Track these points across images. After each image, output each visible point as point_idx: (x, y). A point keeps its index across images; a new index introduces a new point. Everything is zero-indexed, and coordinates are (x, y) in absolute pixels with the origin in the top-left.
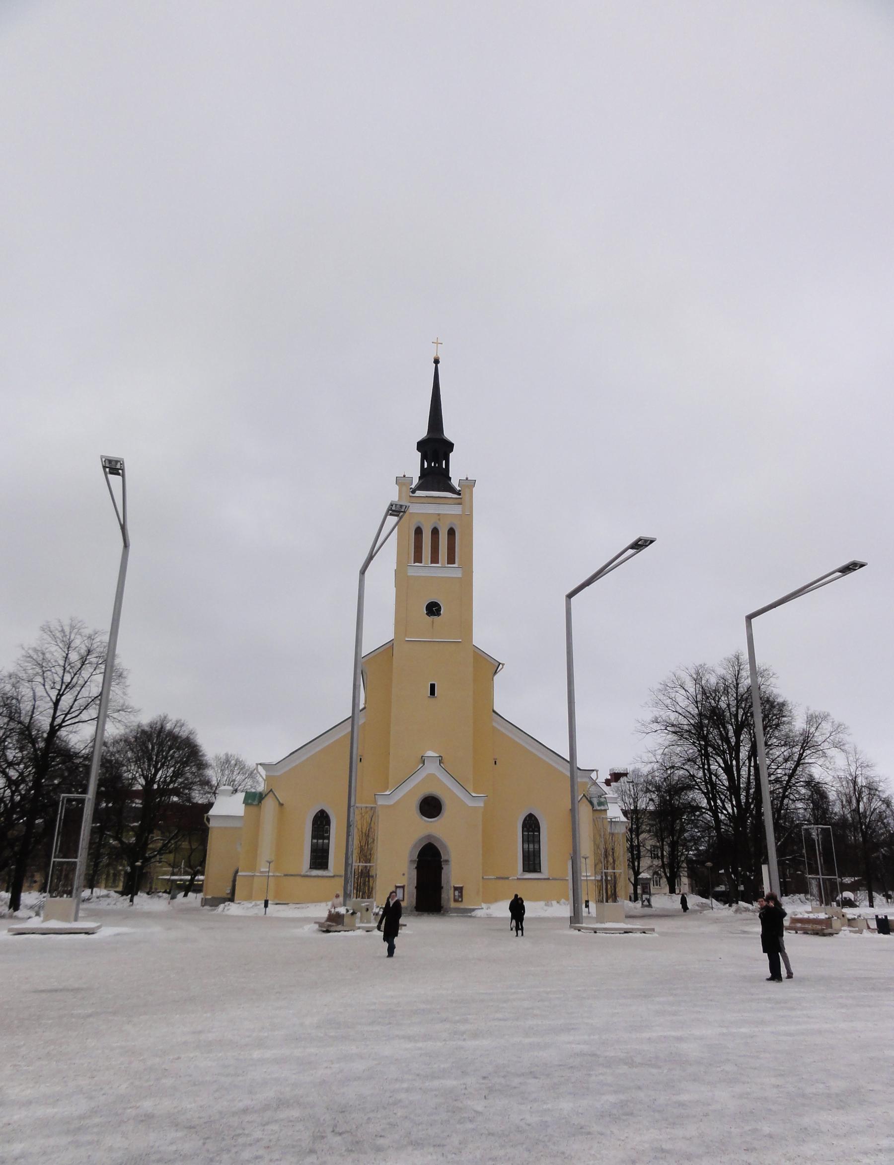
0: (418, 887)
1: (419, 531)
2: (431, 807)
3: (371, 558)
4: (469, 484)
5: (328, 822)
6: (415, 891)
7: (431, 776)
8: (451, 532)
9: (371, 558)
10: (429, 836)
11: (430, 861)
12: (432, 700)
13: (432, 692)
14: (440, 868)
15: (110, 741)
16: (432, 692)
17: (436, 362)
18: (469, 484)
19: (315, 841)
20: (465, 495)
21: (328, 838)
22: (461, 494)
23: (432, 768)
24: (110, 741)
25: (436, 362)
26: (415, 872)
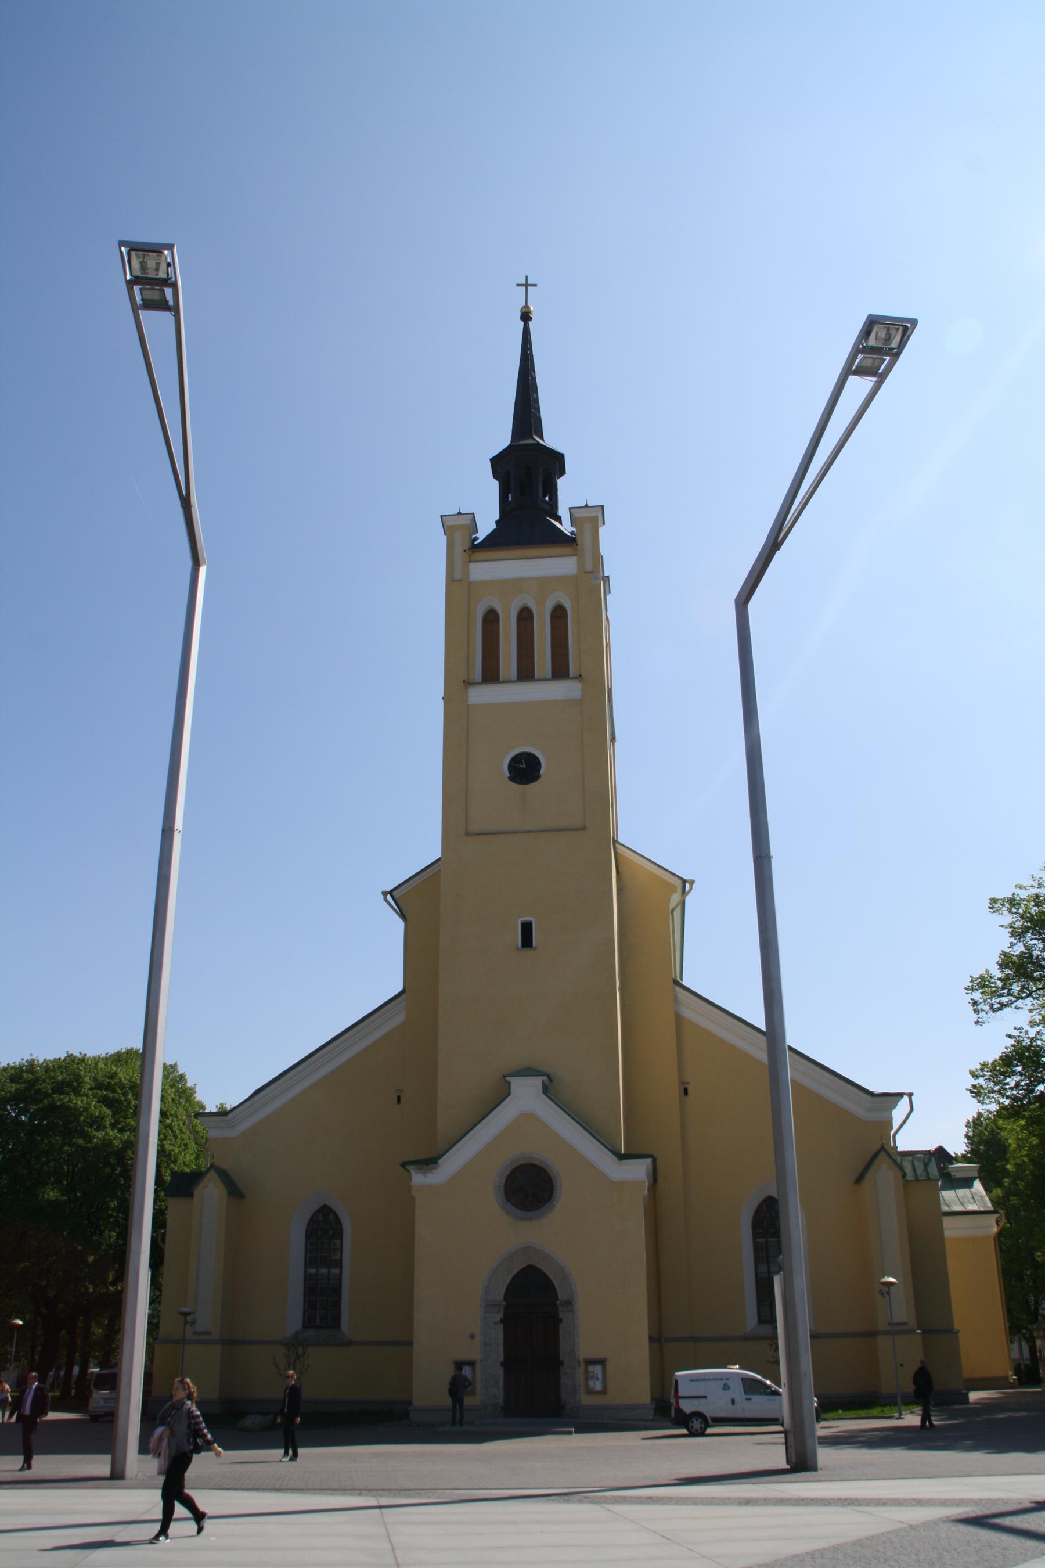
0: (509, 1364)
1: (491, 619)
3: (186, 502)
4: (591, 518)
5: (339, 1233)
6: (500, 1372)
7: (527, 1118)
8: (559, 614)
9: (186, 502)
11: (532, 1306)
12: (528, 952)
13: (527, 940)
14: (556, 1321)
15: (1019, 1350)
16: (527, 940)
17: (526, 317)
18: (591, 518)
19: (313, 1271)
20: (585, 541)
21: (339, 1264)
22: (580, 542)
23: (526, 1096)
24: (1019, 1350)
25: (526, 317)
26: (499, 1332)
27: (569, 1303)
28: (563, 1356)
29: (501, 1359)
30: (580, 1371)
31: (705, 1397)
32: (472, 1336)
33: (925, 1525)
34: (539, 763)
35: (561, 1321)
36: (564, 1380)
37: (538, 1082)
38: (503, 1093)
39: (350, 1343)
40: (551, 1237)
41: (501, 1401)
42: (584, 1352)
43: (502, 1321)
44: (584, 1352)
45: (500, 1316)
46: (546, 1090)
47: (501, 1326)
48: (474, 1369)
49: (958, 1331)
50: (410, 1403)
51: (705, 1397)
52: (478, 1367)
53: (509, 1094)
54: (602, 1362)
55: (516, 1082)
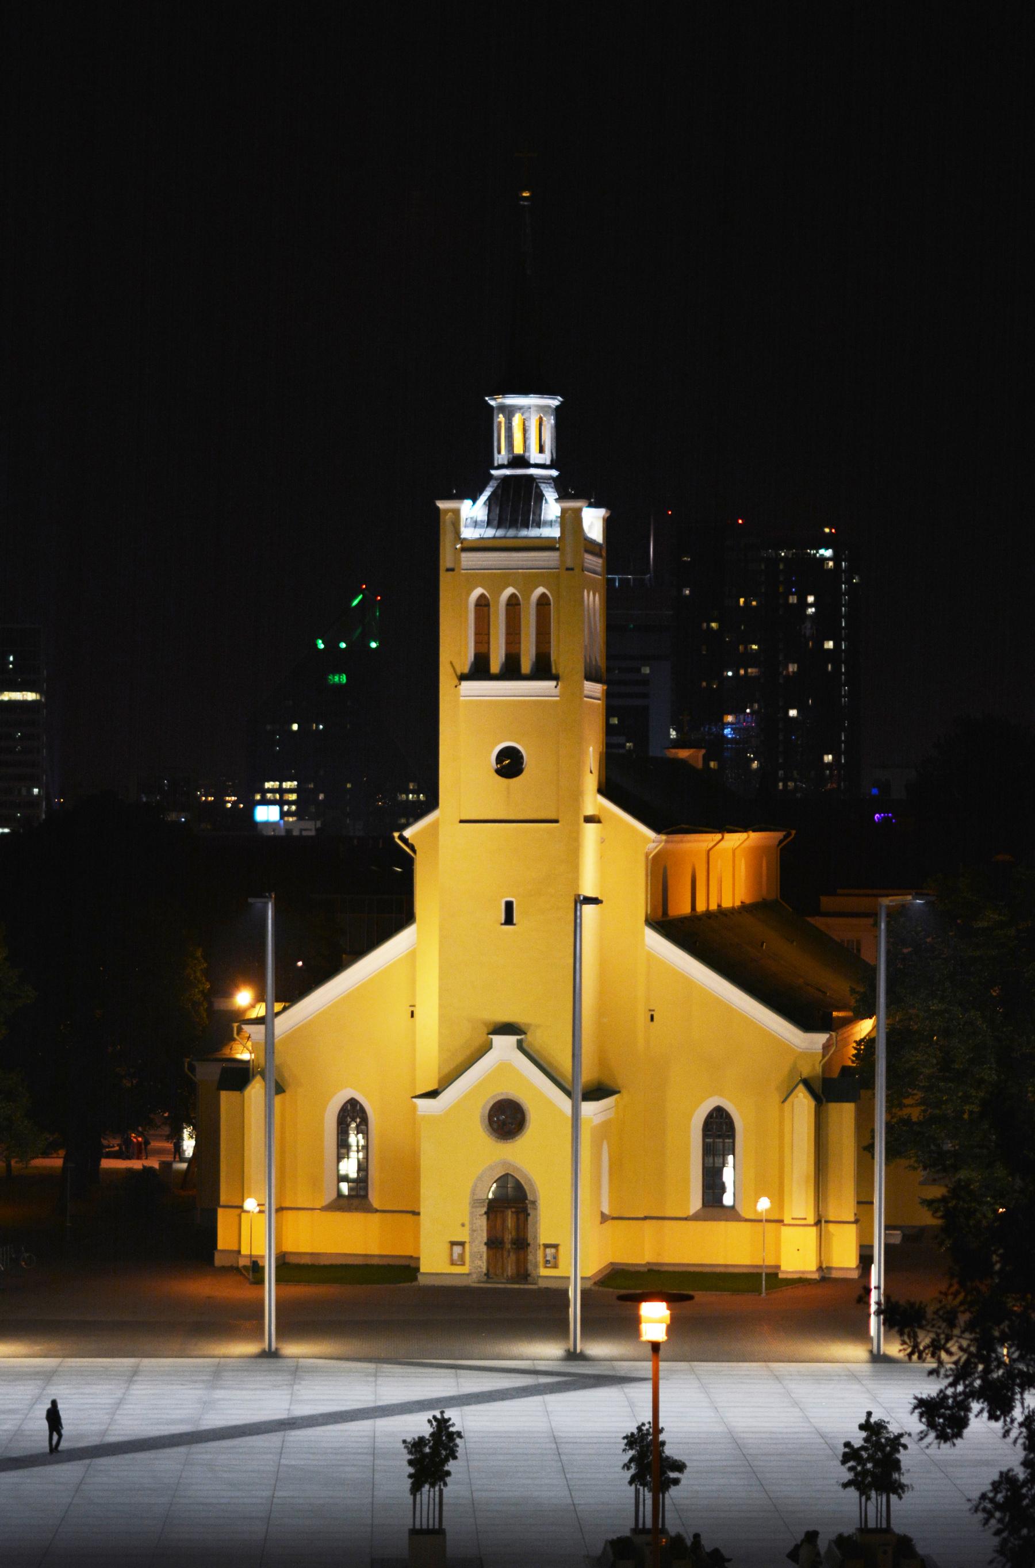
2: (507, 1119)
6: (484, 1249)
7: (504, 1068)
10: (505, 1163)
13: (509, 920)
16: (509, 920)
27: (534, 1203)
28: (530, 1240)
29: (485, 1240)
30: (540, 1253)
31: (462, 821)
32: (463, 1225)
33: (609, 1147)
34: (522, 757)
35: (529, 1215)
36: (530, 1257)
37: (513, 1039)
38: (488, 1047)
39: (377, 1211)
40: (524, 1155)
41: (484, 1270)
42: (543, 1239)
43: (486, 1213)
44: (543, 1239)
45: (485, 1209)
46: (520, 1046)
47: (485, 1217)
48: (464, 1248)
49: (1001, 1473)
50: (418, 1269)
51: (462, 821)
52: (467, 1246)
53: (491, 1048)
54: (556, 1246)
55: (497, 1039)
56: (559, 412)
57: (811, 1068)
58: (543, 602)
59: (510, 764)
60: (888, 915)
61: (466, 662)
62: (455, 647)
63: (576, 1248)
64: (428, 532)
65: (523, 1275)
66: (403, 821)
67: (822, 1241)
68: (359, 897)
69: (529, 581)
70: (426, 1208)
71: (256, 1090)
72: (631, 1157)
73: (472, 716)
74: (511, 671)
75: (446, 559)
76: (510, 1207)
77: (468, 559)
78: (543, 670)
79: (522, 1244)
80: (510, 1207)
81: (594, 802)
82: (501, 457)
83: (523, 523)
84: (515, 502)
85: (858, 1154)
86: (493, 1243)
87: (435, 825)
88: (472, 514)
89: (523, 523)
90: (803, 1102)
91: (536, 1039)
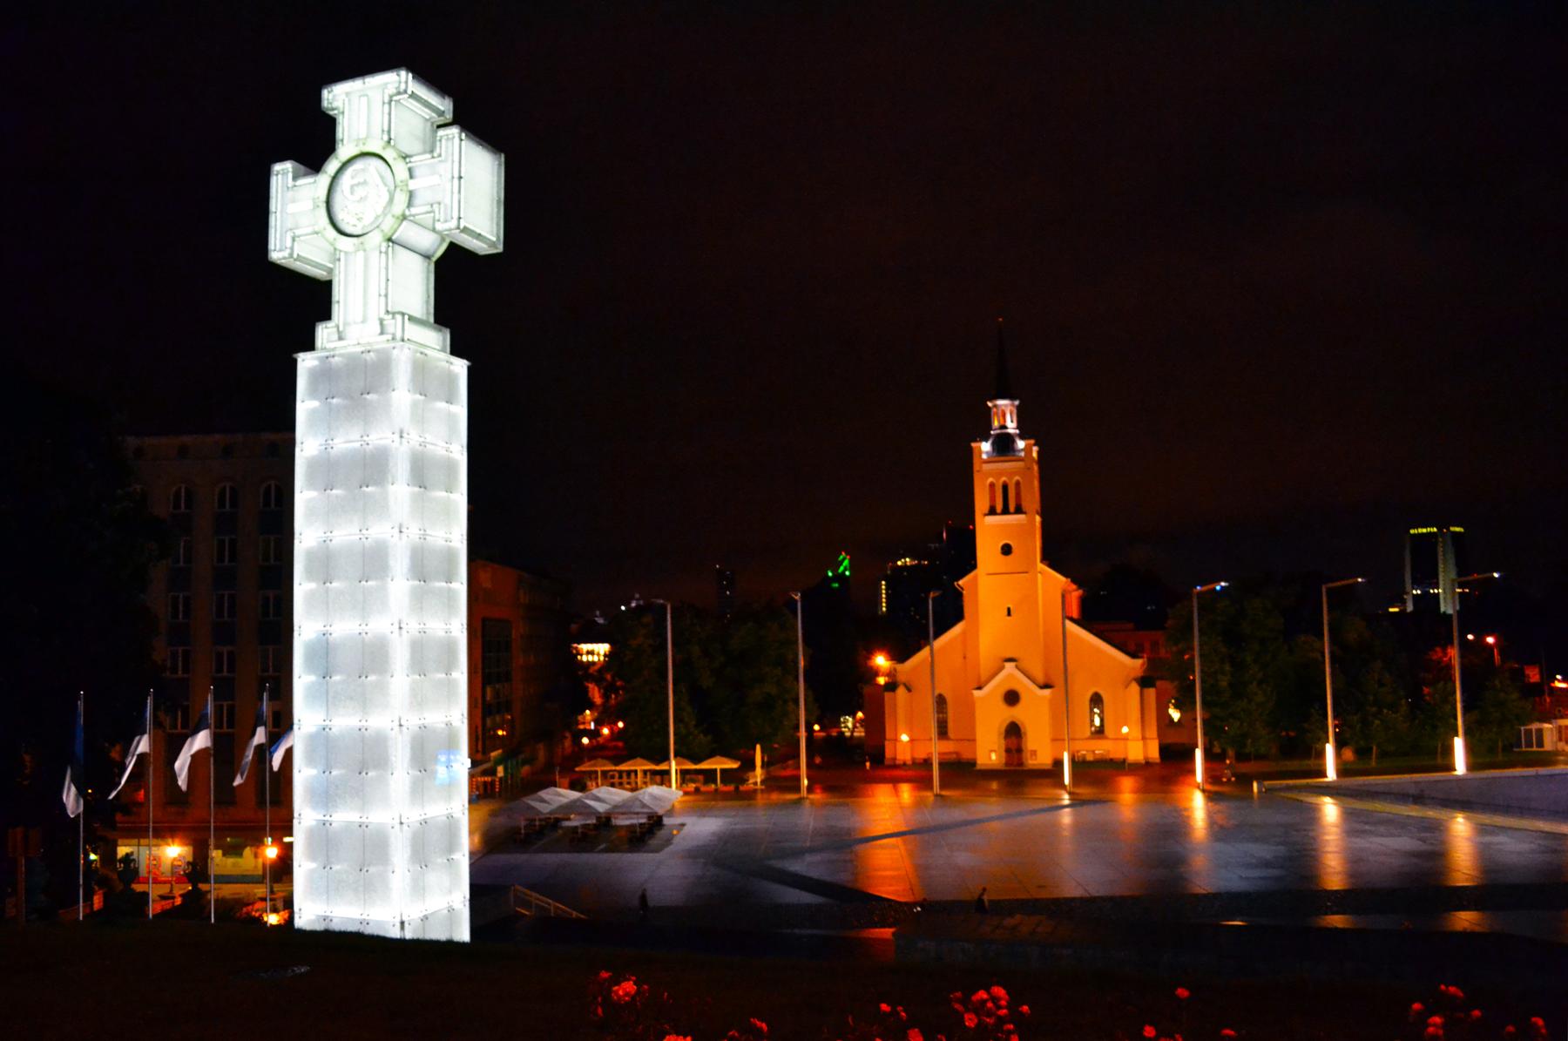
2: (1012, 698)
7: (1010, 676)
13: (1009, 614)
16: (1009, 614)
37: (1012, 664)
38: (1002, 668)
56: (1018, 408)
57: (1139, 673)
58: (1018, 483)
59: (1007, 550)
60: (1201, 609)
61: (986, 509)
62: (981, 502)
63: (1039, 751)
64: (969, 455)
65: (1021, 764)
66: (818, 760)
67: (1145, 746)
68: (929, 604)
69: (1011, 475)
70: (979, 737)
71: (901, 691)
72: (1063, 713)
73: (990, 530)
74: (1006, 511)
75: (976, 467)
76: (1014, 732)
77: (985, 467)
78: (1019, 510)
79: (1019, 750)
80: (1014, 732)
81: (1041, 566)
82: (996, 424)
83: (1003, 455)
84: (1004, 445)
85: (1443, 842)
86: (1008, 751)
87: (976, 578)
88: (986, 447)
89: (1003, 455)
90: (1135, 688)
91: (1025, 664)
